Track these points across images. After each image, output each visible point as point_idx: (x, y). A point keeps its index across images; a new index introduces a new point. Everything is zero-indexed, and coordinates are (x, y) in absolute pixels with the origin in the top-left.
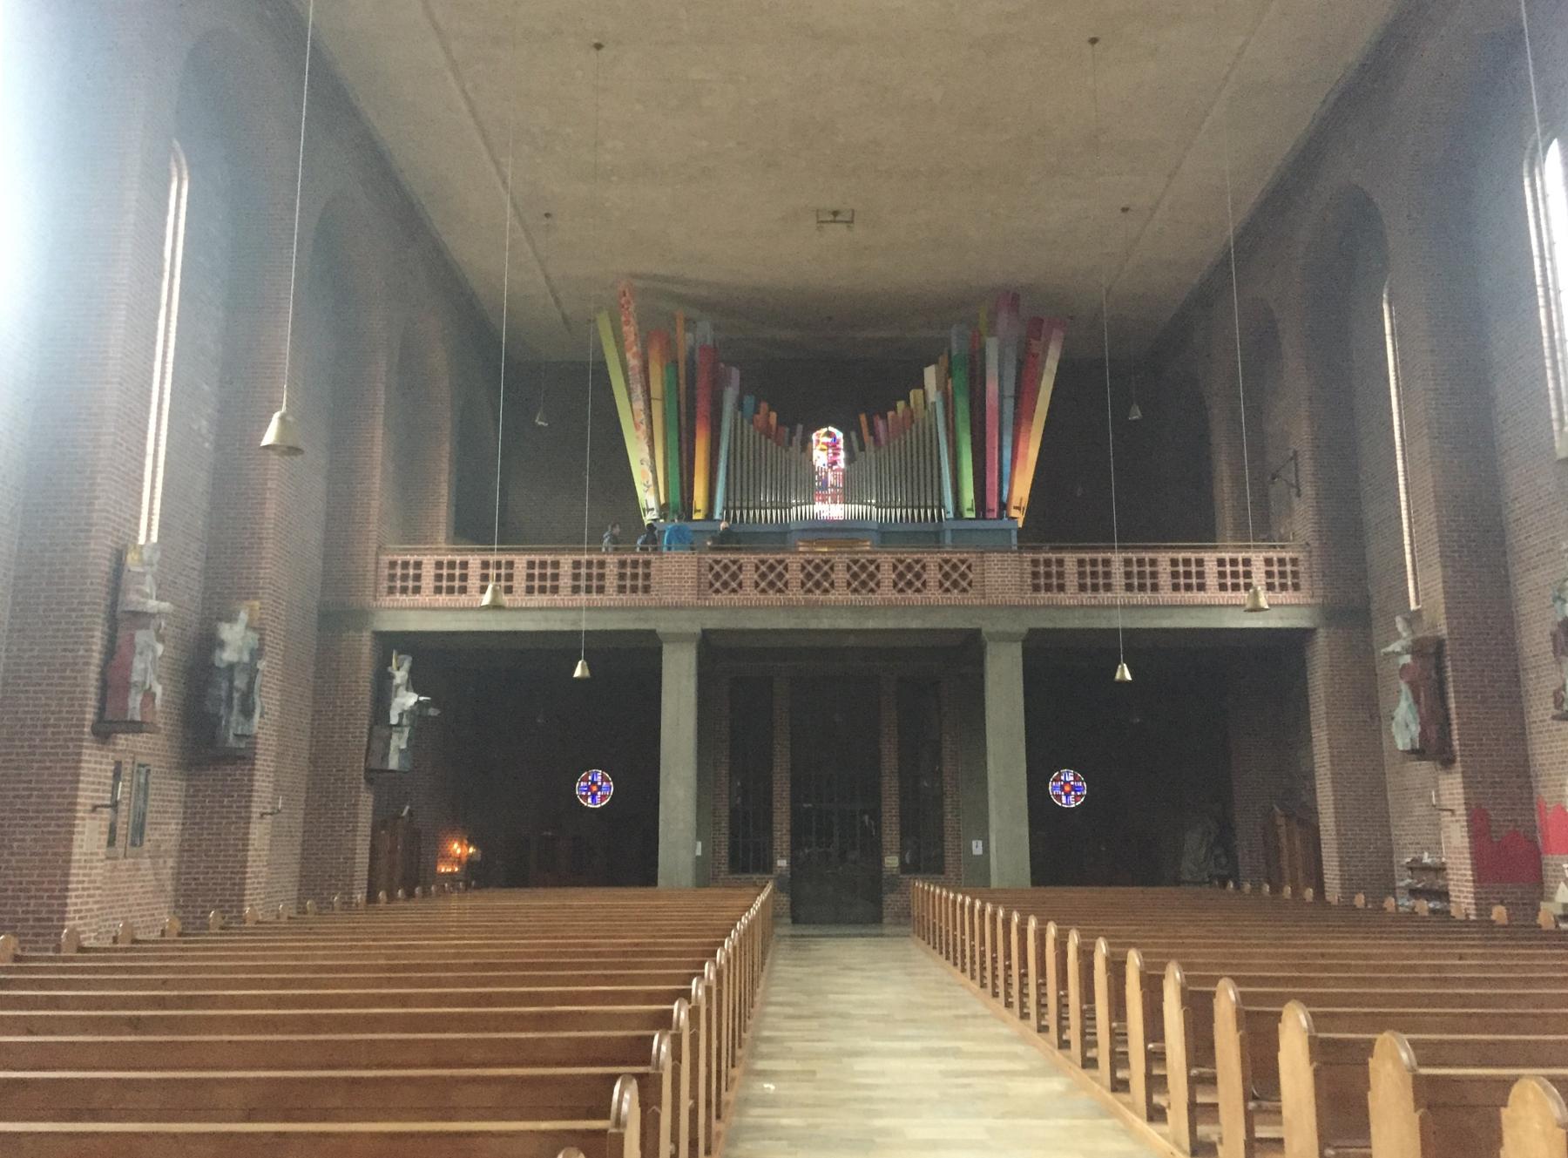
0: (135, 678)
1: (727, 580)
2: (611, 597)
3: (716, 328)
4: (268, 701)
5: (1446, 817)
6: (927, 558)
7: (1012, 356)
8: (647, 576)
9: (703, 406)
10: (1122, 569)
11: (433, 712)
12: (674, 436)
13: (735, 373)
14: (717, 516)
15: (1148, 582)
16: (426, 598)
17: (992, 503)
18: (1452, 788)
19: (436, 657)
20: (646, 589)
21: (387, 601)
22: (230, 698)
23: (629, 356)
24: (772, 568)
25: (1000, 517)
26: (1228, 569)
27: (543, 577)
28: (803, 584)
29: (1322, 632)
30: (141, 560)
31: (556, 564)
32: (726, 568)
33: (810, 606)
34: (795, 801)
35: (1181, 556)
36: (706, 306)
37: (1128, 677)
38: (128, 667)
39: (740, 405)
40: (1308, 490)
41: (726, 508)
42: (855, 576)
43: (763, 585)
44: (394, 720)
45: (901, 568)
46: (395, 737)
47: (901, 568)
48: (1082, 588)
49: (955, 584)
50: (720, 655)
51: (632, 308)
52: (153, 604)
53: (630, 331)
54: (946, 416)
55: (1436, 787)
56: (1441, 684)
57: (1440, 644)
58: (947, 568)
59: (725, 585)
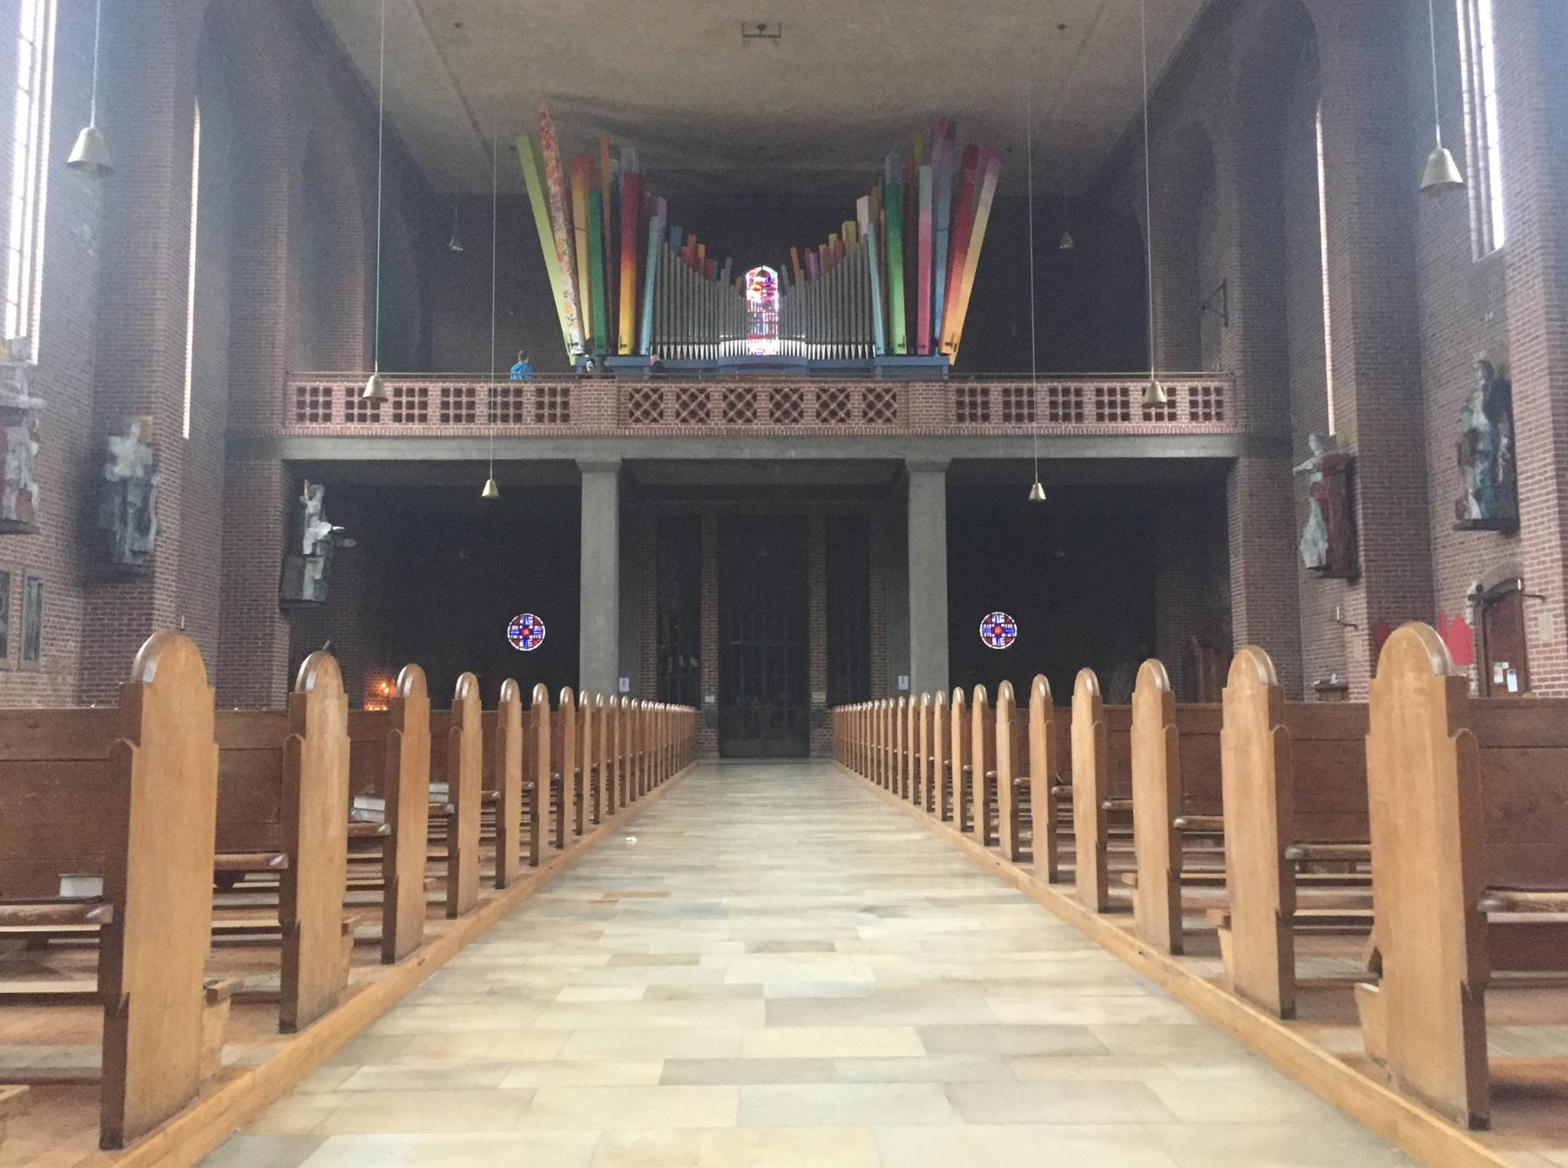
1: (647, 408)
2: (529, 426)
3: (642, 157)
4: (166, 519)
8: (565, 405)
9: (627, 237)
10: (1047, 399)
11: (348, 543)
12: (599, 267)
13: (662, 205)
14: (643, 352)
15: (1073, 412)
17: (924, 339)
19: (350, 488)
20: (565, 418)
21: (298, 429)
22: (124, 514)
23: (550, 182)
24: (693, 397)
25: (932, 353)
27: (458, 405)
28: (725, 414)
29: (1243, 463)
30: (10, 355)
32: (646, 396)
33: (733, 436)
34: (723, 634)
35: (1106, 385)
36: (625, 131)
37: (1042, 496)
39: (667, 235)
40: (1235, 317)
41: (653, 343)
42: (778, 406)
43: (684, 414)
44: (308, 550)
45: (824, 397)
46: (309, 567)
47: (824, 397)
48: (1007, 418)
49: (879, 414)
50: (637, 483)
51: (552, 132)
52: (24, 400)
53: (550, 156)
54: (879, 255)
55: (1341, 601)
56: (1351, 498)
57: (1350, 462)
58: (871, 397)
59: (646, 413)
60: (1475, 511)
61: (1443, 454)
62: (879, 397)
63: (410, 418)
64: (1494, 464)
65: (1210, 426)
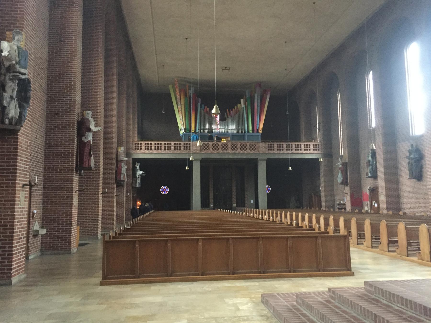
0: (122, 172)
5: (346, 195)
6: (238, 143)
7: (259, 97)
11: (144, 175)
16: (143, 151)
17: (255, 129)
18: (348, 190)
19: (145, 164)
21: (135, 151)
23: (177, 95)
24: (215, 145)
26: (306, 146)
31: (170, 144)
38: (121, 170)
39: (201, 107)
44: (138, 177)
48: (278, 150)
49: (253, 149)
50: (206, 164)
53: (177, 90)
56: (346, 170)
57: (346, 163)
60: (370, 175)
61: (364, 163)
62: (253, 145)
63: (158, 149)
64: (373, 167)
65: (317, 152)
